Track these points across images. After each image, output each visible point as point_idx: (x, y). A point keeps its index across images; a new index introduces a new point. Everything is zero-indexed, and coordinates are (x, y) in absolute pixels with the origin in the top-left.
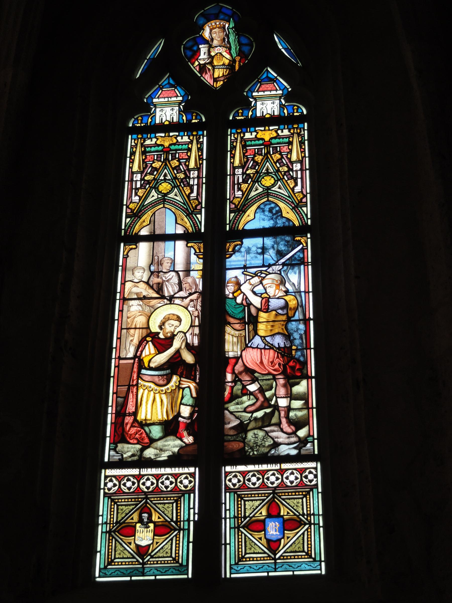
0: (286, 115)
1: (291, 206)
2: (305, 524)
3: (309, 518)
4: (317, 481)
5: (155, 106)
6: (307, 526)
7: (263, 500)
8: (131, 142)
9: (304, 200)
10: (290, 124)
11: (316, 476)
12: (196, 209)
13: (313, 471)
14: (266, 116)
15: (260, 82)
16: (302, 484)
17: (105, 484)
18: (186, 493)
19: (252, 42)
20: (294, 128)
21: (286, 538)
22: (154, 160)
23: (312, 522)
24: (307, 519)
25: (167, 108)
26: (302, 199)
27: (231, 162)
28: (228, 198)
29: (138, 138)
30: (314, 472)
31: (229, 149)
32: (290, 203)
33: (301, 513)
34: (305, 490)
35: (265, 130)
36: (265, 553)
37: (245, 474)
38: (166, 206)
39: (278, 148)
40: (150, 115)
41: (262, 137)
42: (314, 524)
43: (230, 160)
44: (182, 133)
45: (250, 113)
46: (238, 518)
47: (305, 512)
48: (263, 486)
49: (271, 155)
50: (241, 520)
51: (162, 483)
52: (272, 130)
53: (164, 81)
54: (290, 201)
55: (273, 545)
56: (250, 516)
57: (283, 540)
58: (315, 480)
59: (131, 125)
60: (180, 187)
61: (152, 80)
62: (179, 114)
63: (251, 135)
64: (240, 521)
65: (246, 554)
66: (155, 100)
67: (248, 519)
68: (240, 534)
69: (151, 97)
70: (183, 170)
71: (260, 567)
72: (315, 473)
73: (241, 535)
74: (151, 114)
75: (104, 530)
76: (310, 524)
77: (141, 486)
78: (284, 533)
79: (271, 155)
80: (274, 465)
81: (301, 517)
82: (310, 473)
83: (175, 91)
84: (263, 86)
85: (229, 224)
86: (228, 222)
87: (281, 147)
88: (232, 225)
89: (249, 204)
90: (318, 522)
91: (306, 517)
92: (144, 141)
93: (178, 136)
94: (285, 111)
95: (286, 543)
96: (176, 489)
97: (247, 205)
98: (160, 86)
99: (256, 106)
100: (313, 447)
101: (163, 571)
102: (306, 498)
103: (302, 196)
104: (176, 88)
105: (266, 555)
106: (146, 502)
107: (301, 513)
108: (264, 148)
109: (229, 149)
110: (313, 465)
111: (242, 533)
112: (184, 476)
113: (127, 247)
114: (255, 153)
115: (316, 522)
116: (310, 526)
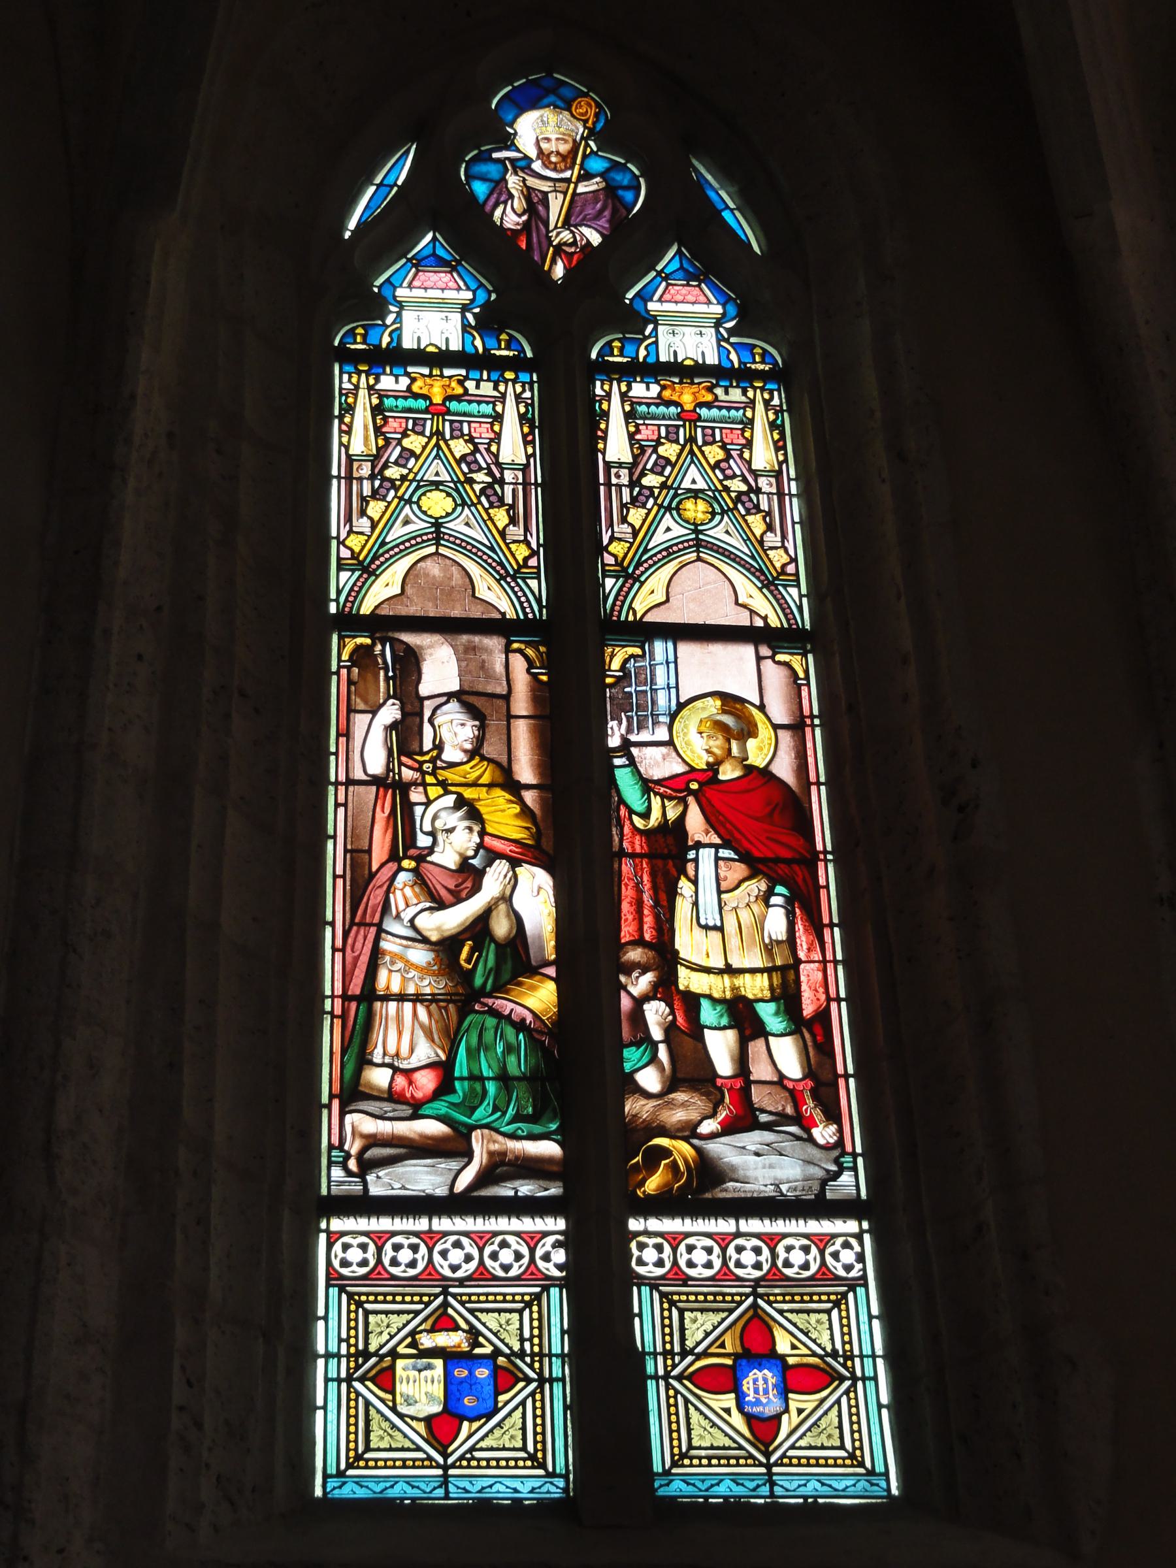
0: (736, 366)
1: (498, 572)
2: (842, 1379)
3: (849, 1363)
4: (864, 1269)
5: (655, 321)
6: (847, 1383)
7: (417, 1313)
8: (341, 382)
9: (533, 562)
10: (496, 369)
11: (861, 1258)
12: (525, 565)
13: (853, 1241)
14: (686, 363)
15: (666, 278)
16: (775, 1274)
17: (861, 1258)
18: (554, 1286)
19: (637, 178)
20: (506, 381)
21: (794, 1412)
22: (407, 429)
23: (859, 1373)
24: (844, 1366)
25: (431, 310)
26: (526, 559)
27: (341, 444)
28: (334, 534)
29: (359, 373)
30: (850, 1246)
31: (336, 413)
32: (494, 564)
33: (829, 1349)
34: (832, 1289)
35: (431, 375)
36: (419, 1449)
37: (383, 1240)
38: (442, 550)
39: (465, 425)
40: (642, 341)
41: (424, 391)
42: (864, 1379)
43: (340, 437)
44: (475, 374)
45: (642, 353)
46: (541, 1355)
47: (839, 1346)
48: (725, 1274)
49: (446, 442)
50: (356, 1361)
51: (835, 1256)
52: (450, 377)
53: (669, 260)
54: (494, 560)
55: (763, 1429)
56: (381, 1352)
57: (785, 1417)
58: (859, 1266)
59: (594, 355)
60: (479, 507)
61: (390, 236)
62: (719, 346)
63: (397, 382)
64: (669, 1362)
65: (368, 1449)
66: (651, 306)
67: (373, 1360)
68: (353, 1396)
69: (644, 297)
70: (484, 465)
71: (714, 1482)
72: (858, 1249)
73: (356, 1400)
74: (646, 338)
75: (333, 1374)
76: (854, 1379)
77: (488, 1263)
78: (786, 1400)
79: (446, 442)
80: (411, 1220)
81: (829, 1359)
82: (847, 1245)
83: (701, 290)
84: (672, 290)
85: (337, 600)
86: (333, 595)
87: (473, 425)
88: (345, 605)
89: (387, 556)
90: (872, 1375)
91: (841, 1360)
92: (377, 380)
93: (466, 378)
94: (733, 356)
95: (794, 1425)
96: (379, 1273)
97: (382, 559)
98: (659, 273)
99: (656, 336)
100: (851, 1183)
101: (428, 1490)
102: (531, 1312)
103: (527, 553)
104: (700, 282)
105: (421, 1455)
106: (445, 1304)
107: (829, 1349)
108: (432, 419)
109: (336, 413)
110: (852, 1226)
111: (358, 1394)
112: (840, 1241)
113: (347, 640)
114: (407, 429)
115: (869, 1372)
116: (854, 1385)
